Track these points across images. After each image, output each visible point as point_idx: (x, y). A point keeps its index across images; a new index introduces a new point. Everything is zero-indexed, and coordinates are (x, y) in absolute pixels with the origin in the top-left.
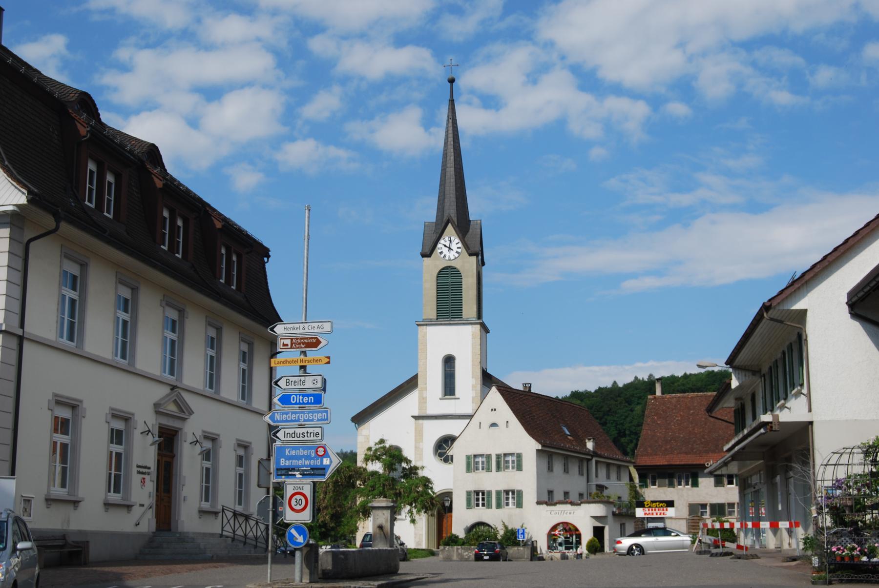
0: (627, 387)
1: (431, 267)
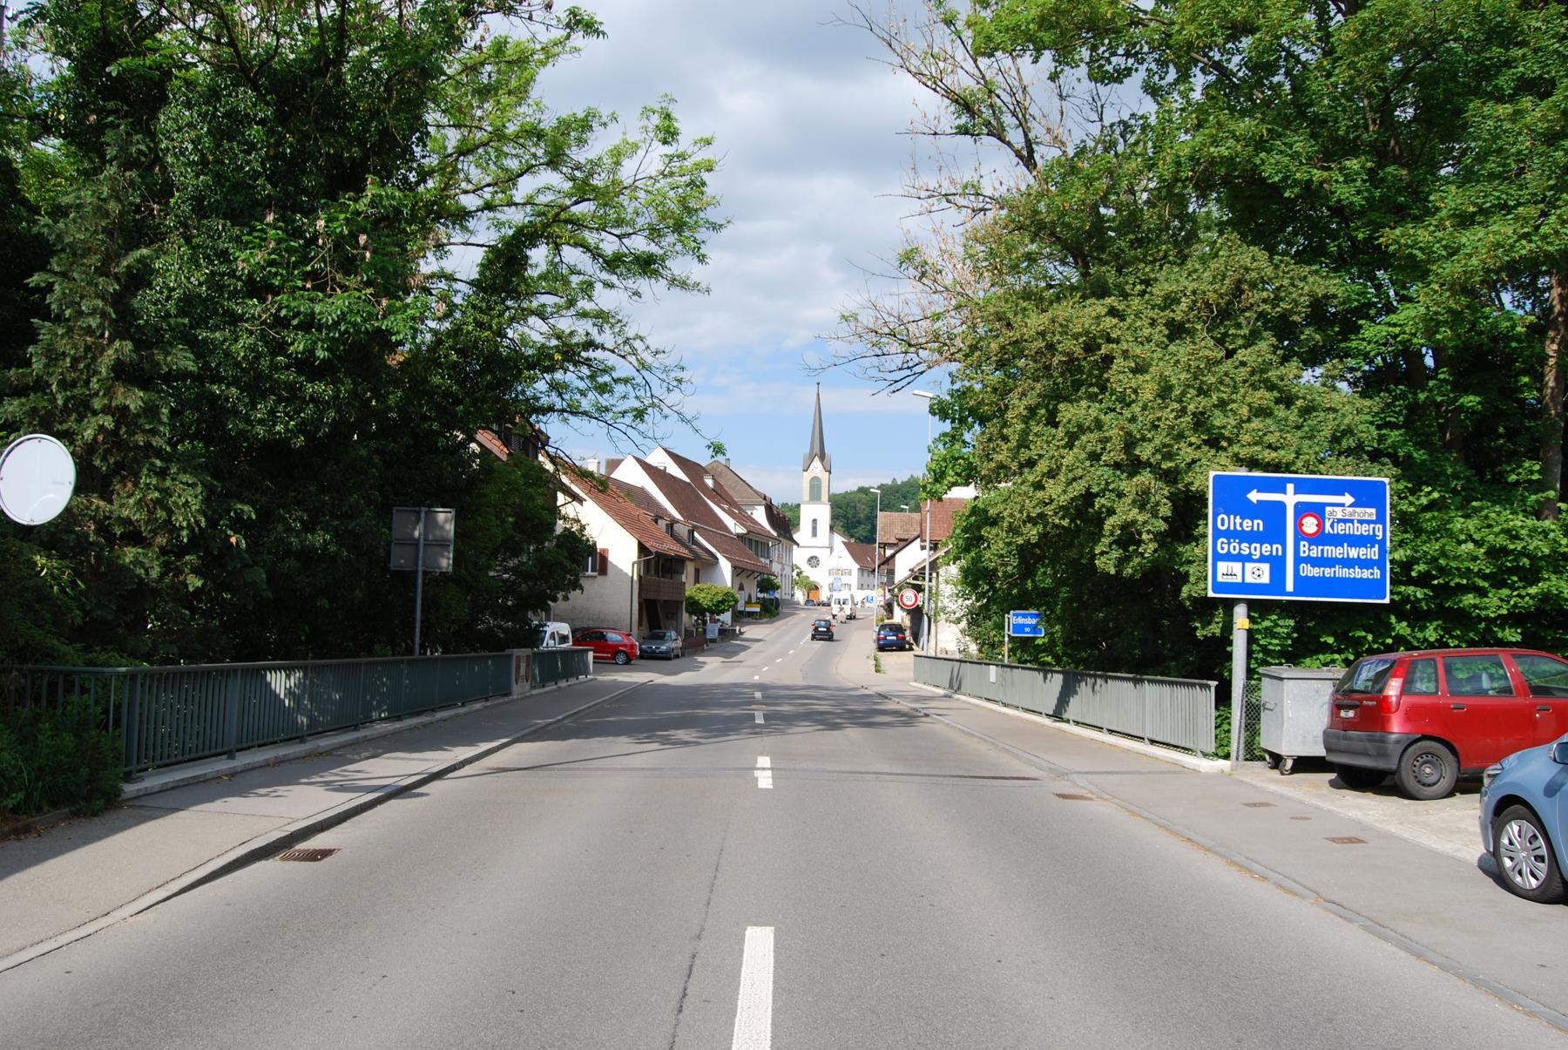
0: (904, 484)
1: (807, 476)
